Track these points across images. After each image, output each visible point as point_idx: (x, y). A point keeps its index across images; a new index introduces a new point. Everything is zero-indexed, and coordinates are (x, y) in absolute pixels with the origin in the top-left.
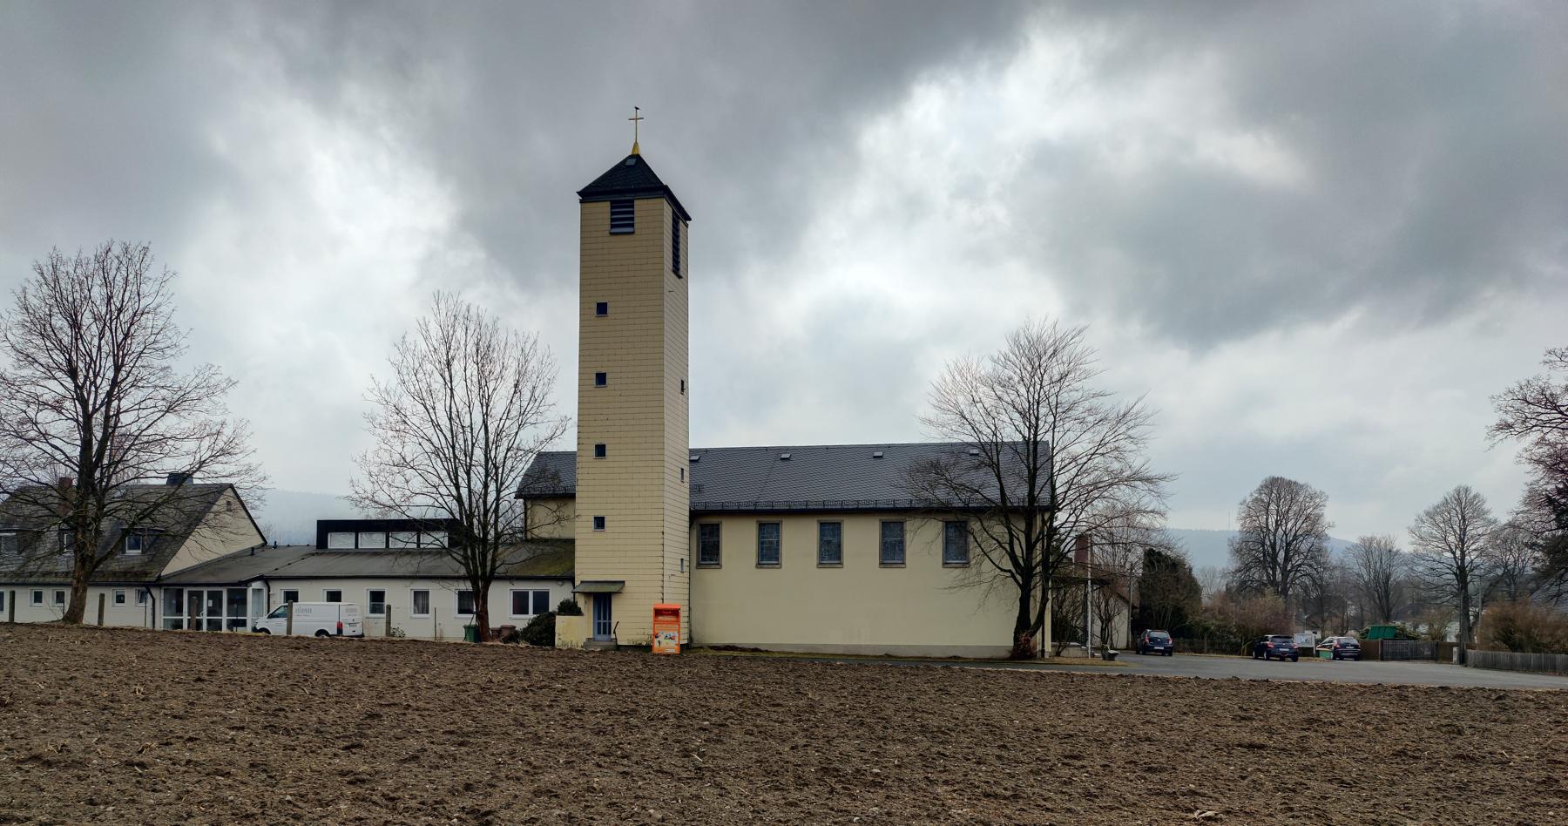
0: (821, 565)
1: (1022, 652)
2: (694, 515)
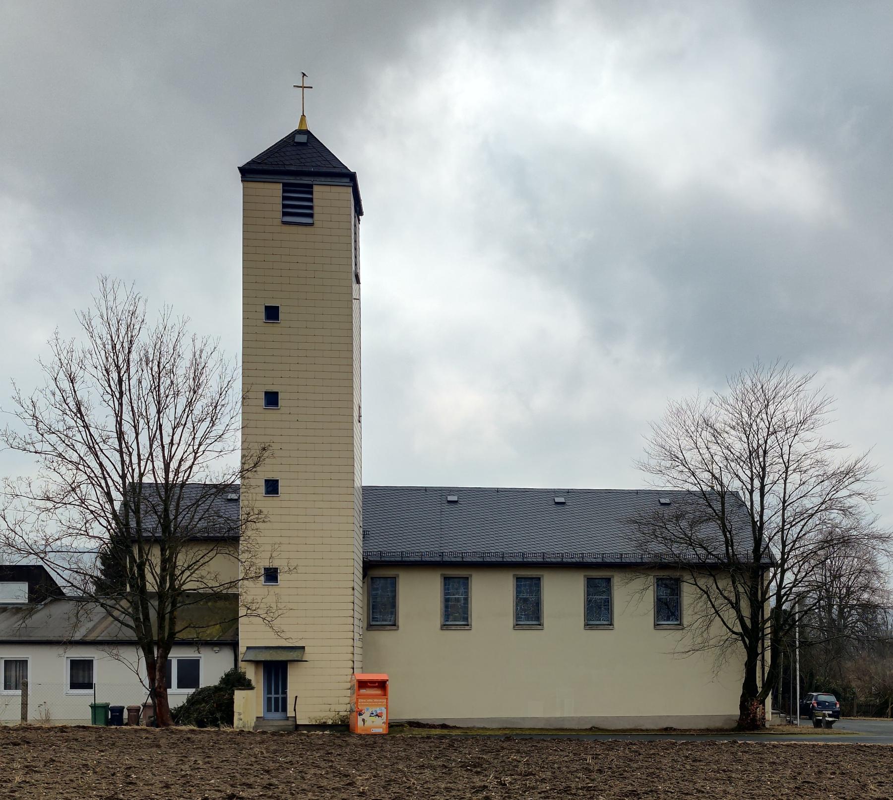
0: (517, 626)
1: (749, 722)
2: (369, 566)
